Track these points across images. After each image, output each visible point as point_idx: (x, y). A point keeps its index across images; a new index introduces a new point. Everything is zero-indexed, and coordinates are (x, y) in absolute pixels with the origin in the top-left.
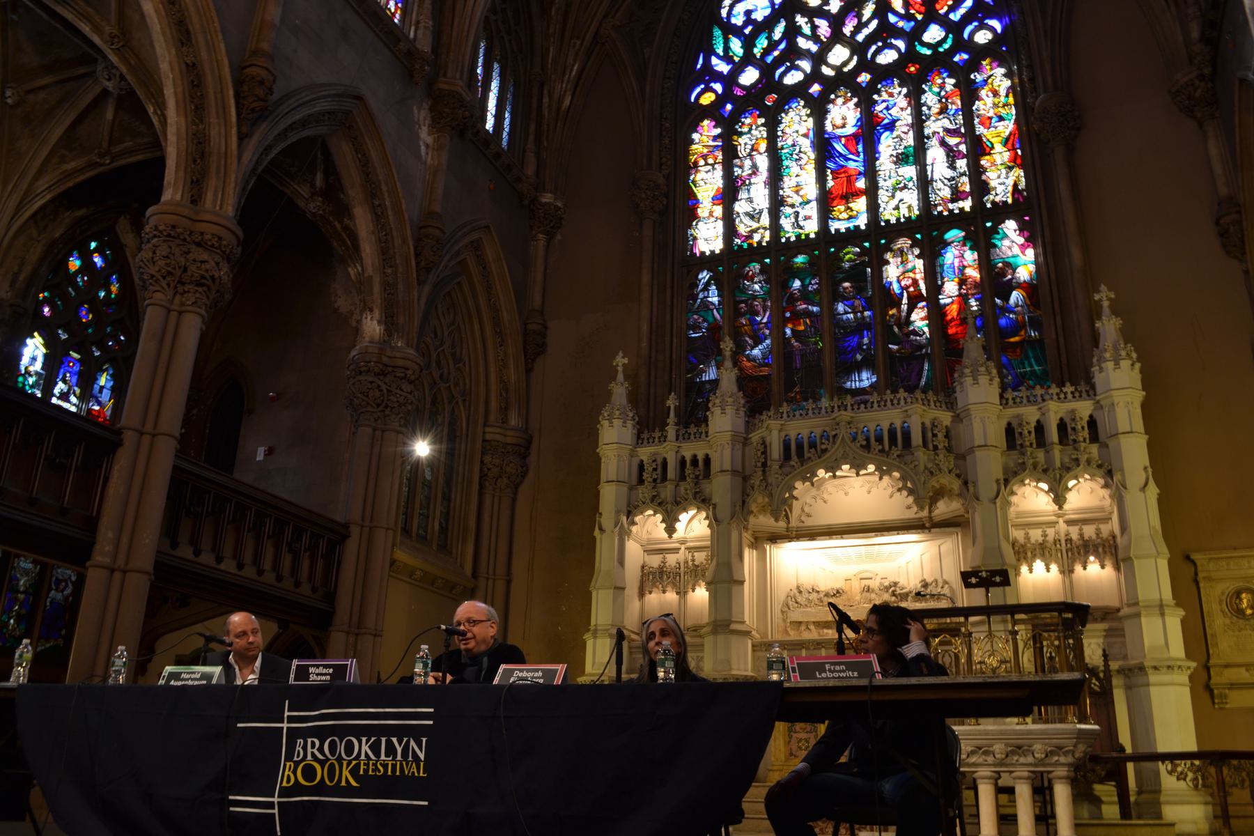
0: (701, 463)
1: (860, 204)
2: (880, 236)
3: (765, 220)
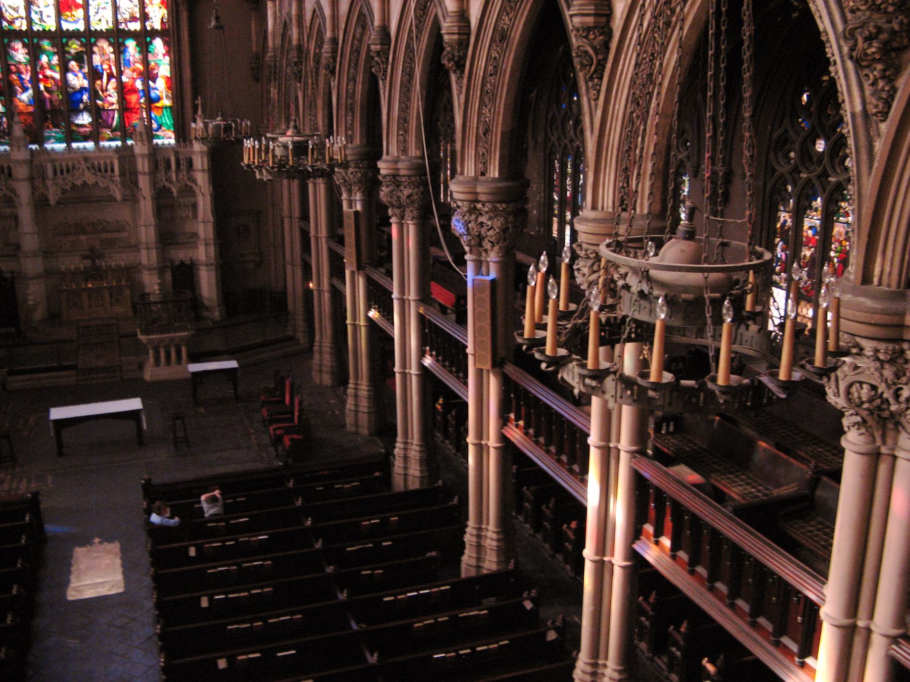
0: (6, 172)
1: (80, 13)
2: (89, 37)
3: (23, 13)
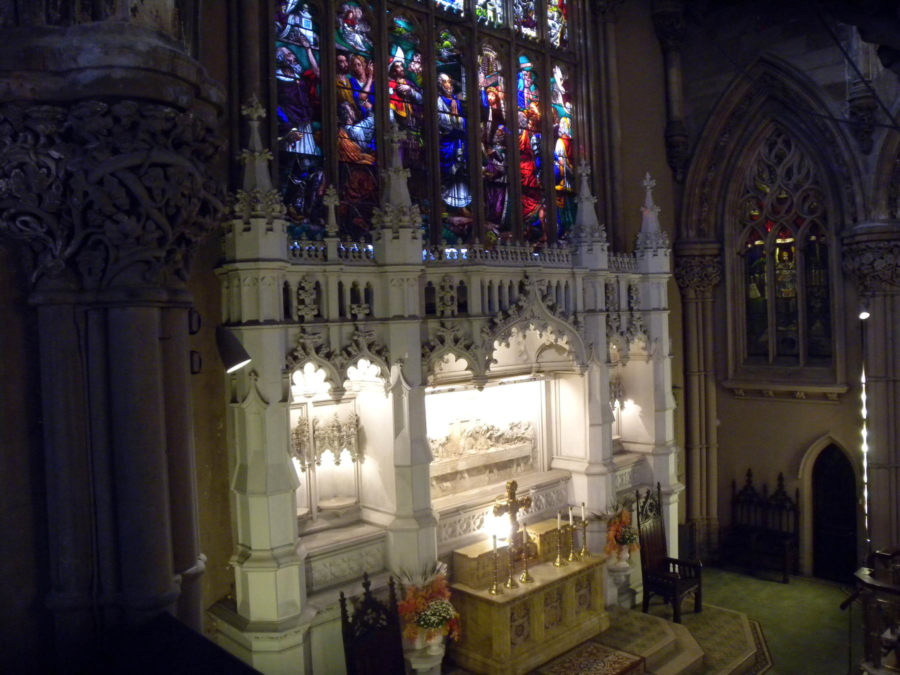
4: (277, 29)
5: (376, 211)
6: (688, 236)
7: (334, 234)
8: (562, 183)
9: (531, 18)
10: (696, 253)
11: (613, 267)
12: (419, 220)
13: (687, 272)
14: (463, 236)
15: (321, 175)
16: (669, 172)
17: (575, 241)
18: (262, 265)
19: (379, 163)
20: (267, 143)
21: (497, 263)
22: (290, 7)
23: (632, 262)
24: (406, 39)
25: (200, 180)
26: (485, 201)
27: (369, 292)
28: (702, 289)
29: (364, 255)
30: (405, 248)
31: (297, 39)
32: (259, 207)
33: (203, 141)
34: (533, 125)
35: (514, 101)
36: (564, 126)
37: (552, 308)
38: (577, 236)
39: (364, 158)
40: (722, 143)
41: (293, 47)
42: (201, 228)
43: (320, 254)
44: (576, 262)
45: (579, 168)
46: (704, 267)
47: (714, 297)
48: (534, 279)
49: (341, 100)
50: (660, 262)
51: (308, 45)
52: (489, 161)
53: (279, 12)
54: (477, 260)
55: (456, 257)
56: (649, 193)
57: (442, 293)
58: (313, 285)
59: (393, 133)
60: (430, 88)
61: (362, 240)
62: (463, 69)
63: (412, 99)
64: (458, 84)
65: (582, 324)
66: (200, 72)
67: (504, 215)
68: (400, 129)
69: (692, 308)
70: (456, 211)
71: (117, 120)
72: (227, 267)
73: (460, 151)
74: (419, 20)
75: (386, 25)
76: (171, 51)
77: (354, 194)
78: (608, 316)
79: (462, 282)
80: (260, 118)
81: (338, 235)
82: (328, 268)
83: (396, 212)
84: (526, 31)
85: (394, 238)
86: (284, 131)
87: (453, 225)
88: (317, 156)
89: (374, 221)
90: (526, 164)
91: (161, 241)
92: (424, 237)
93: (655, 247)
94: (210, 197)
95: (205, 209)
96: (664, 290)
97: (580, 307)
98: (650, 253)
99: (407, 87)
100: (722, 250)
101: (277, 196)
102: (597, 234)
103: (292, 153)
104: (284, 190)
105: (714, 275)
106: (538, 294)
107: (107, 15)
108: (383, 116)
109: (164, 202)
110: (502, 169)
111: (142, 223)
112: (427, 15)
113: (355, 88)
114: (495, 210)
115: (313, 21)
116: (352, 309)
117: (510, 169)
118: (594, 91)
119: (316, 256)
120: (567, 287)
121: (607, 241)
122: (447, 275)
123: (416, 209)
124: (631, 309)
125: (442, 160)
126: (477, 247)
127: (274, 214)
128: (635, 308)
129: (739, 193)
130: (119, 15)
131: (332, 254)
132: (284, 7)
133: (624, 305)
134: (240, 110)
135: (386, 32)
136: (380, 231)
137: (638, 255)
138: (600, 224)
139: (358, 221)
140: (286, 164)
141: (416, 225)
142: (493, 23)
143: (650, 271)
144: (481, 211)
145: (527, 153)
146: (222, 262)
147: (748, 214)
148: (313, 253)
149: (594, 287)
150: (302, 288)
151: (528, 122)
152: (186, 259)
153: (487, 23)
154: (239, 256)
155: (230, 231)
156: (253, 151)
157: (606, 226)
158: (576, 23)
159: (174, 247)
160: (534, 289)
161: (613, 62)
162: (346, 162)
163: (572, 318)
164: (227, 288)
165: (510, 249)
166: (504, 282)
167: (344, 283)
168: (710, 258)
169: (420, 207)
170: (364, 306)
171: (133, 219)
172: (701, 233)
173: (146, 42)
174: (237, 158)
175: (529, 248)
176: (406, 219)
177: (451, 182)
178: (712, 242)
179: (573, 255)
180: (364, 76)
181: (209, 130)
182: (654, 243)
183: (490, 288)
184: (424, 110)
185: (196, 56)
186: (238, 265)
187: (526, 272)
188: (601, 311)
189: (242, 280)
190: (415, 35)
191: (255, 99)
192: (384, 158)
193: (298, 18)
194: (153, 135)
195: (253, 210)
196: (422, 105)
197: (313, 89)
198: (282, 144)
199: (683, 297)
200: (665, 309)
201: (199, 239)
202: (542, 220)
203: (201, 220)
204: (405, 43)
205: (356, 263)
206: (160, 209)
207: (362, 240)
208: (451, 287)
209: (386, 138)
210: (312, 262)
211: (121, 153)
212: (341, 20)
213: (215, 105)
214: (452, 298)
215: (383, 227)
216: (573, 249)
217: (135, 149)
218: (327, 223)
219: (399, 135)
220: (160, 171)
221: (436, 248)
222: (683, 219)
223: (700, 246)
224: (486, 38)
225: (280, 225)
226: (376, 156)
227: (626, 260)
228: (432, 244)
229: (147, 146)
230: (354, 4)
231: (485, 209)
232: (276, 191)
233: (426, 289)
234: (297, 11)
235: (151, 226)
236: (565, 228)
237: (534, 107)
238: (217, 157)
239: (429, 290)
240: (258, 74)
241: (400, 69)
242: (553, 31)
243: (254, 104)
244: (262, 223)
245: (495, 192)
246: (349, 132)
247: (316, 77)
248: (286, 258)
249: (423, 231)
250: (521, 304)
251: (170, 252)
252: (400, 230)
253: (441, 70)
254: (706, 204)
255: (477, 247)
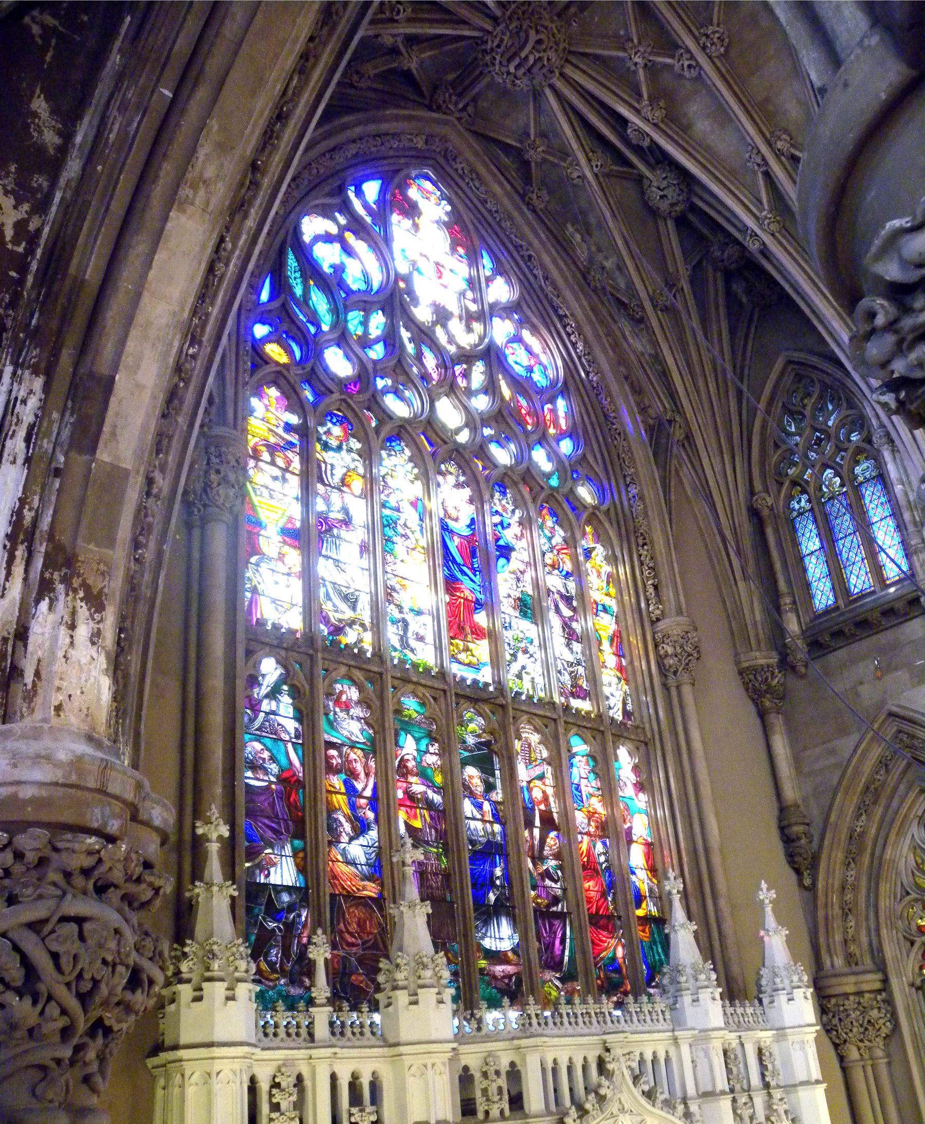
2: (497, 703)
3: (365, 615)
4: (246, 719)
5: (383, 964)
6: (832, 966)
7: (325, 1001)
8: (644, 905)
9: (581, 687)
10: (850, 989)
11: (734, 1024)
12: (446, 974)
13: (840, 1020)
14: (512, 992)
15: (304, 914)
16: (793, 877)
17: (672, 989)
18: (217, 1052)
19: (386, 894)
20: (231, 874)
21: (562, 1031)
22: (264, 690)
23: (758, 1012)
24: (419, 724)
25: (130, 937)
26: (539, 940)
27: (375, 1087)
28: (867, 1043)
29: (367, 1030)
30: (425, 1015)
31: (273, 732)
32: (216, 965)
33: (139, 880)
34: (597, 827)
35: (569, 800)
36: (640, 827)
37: (649, 1095)
38: (674, 981)
39: (364, 888)
40: (858, 830)
41: (268, 742)
42: (128, 1008)
43: (303, 1031)
44: (677, 1022)
45: (666, 883)
46: (864, 1011)
47: (888, 1055)
48: (617, 1052)
49: (331, 809)
50: (798, 1009)
51: (287, 738)
52: (540, 883)
53: (250, 698)
54: (533, 1030)
55: (501, 1027)
56: (769, 910)
57: (485, 1083)
58: (292, 1080)
59: (405, 852)
60: (453, 789)
61: (365, 1008)
62: (496, 759)
63: (430, 805)
64: (491, 779)
65: (698, 1117)
66: (139, 786)
67: (566, 959)
68: (415, 846)
69: (858, 1076)
70: (496, 957)
71: (19, 856)
72: (164, 1056)
73: (498, 872)
74: (435, 699)
75: (391, 707)
76: (102, 760)
77: (351, 940)
78: (734, 1100)
79: (512, 1064)
80: (220, 838)
81: (331, 1001)
82: (315, 1053)
83: (413, 964)
84: (576, 703)
85: (411, 1003)
86: (252, 854)
87: (495, 977)
88: (299, 889)
89: (381, 978)
90: (591, 883)
91: (66, 1033)
92: (455, 999)
93: (788, 987)
94: (146, 964)
95: (136, 980)
96: (812, 1051)
97: (691, 1091)
98: (782, 997)
99: (422, 788)
100: (886, 981)
101: (242, 949)
102: (702, 977)
103: (264, 884)
104: (253, 938)
105: (881, 1021)
106: (627, 1073)
107: (22, 716)
108: (389, 828)
109: (75, 974)
110: (559, 892)
111: (39, 1007)
112: (445, 691)
113: (351, 791)
114: (552, 952)
115: (296, 709)
116: (351, 1115)
117: (570, 893)
118: (675, 776)
119: (298, 1034)
120: (667, 1060)
121: (719, 985)
122: (490, 1054)
123: (441, 958)
124: (767, 1086)
125: (474, 885)
126: (532, 1009)
127: (237, 974)
128: (773, 1083)
129: (895, 898)
130: (38, 715)
131: (322, 1030)
132: (256, 690)
133: (755, 1080)
134: (194, 827)
135: (391, 715)
136: (391, 994)
137: (766, 1001)
138: (705, 961)
139: (360, 979)
140: (255, 900)
141: (443, 982)
142: (532, 697)
143: (787, 1024)
144: (534, 955)
145: (591, 868)
146: (158, 1048)
147: (914, 927)
148: (293, 1031)
149: (707, 1055)
150: (276, 1085)
151: (589, 825)
152: (102, 1058)
153: (523, 697)
154: (184, 1040)
155: (173, 1001)
156: (209, 885)
157: (714, 963)
158: (641, 688)
159: (86, 1039)
160: (620, 1067)
161: (695, 734)
162: (340, 894)
163: (680, 1108)
164: (164, 1088)
165: (579, 1009)
166: (574, 1060)
167: (339, 1075)
168: (872, 996)
169: (446, 955)
170: (369, 1109)
171: (28, 1001)
172: (850, 958)
173: (69, 749)
174: (187, 894)
175: (607, 1005)
176: (428, 973)
177: (488, 914)
178: (869, 972)
179: (671, 1009)
180: (362, 775)
181: (147, 865)
182: (787, 982)
183: (554, 1070)
184: (445, 819)
185: (135, 765)
186: (182, 1053)
187: (605, 1042)
188: (723, 1093)
189: (187, 1077)
190: (432, 719)
191: (214, 812)
192: (394, 887)
193: (274, 703)
194: (68, 875)
195: (208, 969)
196: (444, 811)
197: (293, 796)
198: (250, 872)
199: (841, 1058)
200: (817, 1082)
201: (124, 1026)
202: (621, 961)
203: (128, 996)
204: (416, 729)
205: (357, 1043)
206: (68, 985)
207: (365, 1008)
208: (497, 1073)
209: (395, 860)
210: (292, 1045)
211: (20, 902)
212: (331, 704)
213: (157, 830)
214: (500, 1089)
215: (395, 988)
216: (671, 1001)
217: (40, 897)
218: (313, 984)
219: (413, 855)
220: (74, 927)
221: (472, 1015)
222: (822, 940)
223: (852, 979)
224: (525, 717)
225: (246, 990)
226: (382, 885)
227: (750, 1010)
228: (466, 1009)
229: (59, 892)
230: (349, 682)
231: (539, 950)
232: (241, 941)
233: (460, 1077)
234: (274, 694)
235: (53, 1010)
236: (653, 972)
237: (596, 804)
238: (158, 902)
239: (465, 1079)
240: (220, 782)
241: (411, 764)
242: (612, 702)
243: (213, 819)
244: (218, 990)
245: (551, 925)
246: (344, 853)
247: (298, 781)
248: (253, 1040)
249: (452, 991)
250: (602, 1092)
251: (79, 1049)
252: (419, 991)
253: (465, 763)
254: (850, 917)
255: (532, 1009)
